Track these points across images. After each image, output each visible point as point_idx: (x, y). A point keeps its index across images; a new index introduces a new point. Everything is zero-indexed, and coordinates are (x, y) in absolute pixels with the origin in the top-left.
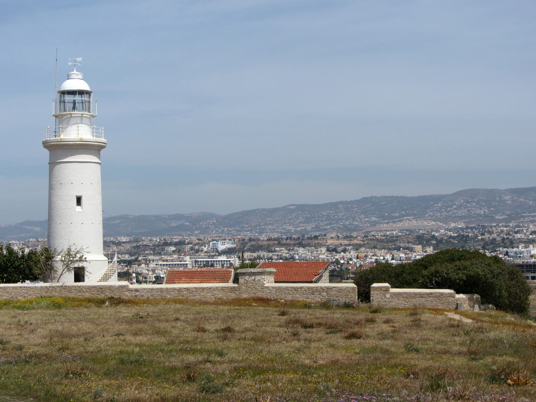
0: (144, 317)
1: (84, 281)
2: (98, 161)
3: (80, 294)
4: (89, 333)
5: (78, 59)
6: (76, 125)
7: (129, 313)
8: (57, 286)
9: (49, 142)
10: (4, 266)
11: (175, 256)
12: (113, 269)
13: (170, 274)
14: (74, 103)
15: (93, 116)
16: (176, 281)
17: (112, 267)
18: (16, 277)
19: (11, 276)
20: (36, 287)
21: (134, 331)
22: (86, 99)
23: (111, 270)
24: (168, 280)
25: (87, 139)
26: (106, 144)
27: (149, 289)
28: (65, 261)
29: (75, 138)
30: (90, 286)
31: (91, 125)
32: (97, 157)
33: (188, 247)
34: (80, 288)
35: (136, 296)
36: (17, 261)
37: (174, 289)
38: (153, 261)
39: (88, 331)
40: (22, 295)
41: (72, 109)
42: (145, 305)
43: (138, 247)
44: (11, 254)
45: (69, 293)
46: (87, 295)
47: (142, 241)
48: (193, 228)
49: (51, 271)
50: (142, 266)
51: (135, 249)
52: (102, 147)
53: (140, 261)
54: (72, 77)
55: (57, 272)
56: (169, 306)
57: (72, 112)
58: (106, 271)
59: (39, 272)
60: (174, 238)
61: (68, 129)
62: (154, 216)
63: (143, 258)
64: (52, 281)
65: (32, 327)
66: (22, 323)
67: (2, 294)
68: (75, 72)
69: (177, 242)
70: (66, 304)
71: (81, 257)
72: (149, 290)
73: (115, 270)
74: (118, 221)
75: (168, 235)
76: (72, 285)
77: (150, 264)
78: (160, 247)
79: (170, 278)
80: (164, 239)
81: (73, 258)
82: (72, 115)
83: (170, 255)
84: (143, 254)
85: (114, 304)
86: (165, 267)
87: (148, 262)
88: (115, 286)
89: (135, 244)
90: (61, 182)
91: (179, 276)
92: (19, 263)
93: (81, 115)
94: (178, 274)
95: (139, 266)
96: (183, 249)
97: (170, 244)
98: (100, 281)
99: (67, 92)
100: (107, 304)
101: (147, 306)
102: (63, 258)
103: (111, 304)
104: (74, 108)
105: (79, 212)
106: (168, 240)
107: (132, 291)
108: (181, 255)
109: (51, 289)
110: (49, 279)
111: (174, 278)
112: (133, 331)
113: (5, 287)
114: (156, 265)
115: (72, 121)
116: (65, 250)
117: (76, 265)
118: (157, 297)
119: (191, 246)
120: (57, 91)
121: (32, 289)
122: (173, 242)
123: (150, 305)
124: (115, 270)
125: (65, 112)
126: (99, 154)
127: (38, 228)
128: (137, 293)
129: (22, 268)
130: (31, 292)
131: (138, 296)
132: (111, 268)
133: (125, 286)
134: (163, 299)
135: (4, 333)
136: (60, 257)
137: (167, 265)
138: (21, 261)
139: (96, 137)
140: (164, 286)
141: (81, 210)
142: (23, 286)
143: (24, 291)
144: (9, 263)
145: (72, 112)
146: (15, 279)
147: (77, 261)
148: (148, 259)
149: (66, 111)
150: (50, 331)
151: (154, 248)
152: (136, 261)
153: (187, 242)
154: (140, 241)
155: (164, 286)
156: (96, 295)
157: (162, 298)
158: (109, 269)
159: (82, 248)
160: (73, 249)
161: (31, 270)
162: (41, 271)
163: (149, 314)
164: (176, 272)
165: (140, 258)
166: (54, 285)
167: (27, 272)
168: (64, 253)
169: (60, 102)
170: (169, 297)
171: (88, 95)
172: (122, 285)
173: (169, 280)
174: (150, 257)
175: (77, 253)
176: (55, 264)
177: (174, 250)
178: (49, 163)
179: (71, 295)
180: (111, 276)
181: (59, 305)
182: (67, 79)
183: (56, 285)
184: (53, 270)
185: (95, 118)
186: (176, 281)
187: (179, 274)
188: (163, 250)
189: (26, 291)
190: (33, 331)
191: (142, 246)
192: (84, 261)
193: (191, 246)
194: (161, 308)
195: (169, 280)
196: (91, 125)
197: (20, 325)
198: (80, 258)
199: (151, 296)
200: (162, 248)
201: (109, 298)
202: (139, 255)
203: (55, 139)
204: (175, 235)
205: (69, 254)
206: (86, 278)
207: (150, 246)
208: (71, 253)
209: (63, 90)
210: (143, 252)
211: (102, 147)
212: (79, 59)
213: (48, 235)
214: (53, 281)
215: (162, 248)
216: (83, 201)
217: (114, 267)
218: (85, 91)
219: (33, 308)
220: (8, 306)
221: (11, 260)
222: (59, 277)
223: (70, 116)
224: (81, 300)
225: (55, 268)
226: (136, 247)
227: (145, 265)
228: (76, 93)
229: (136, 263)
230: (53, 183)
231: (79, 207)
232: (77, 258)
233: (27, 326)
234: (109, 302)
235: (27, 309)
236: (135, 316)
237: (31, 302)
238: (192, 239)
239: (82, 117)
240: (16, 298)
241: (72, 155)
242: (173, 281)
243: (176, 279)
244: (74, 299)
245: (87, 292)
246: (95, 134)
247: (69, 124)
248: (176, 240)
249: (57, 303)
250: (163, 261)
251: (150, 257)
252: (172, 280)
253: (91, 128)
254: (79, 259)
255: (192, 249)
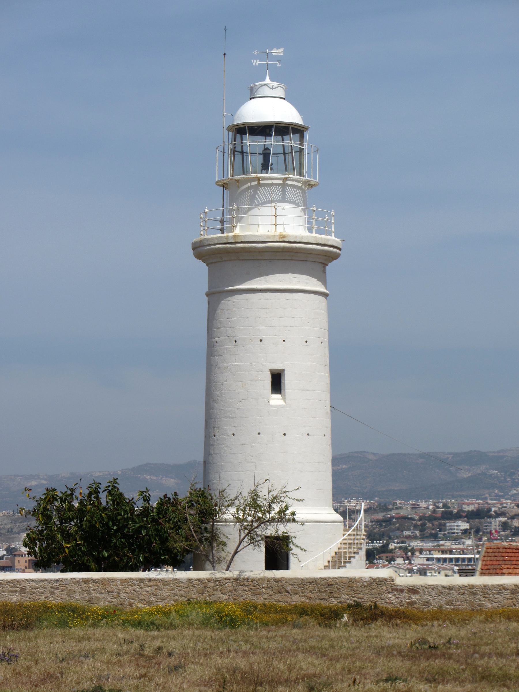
0: (440, 647)
1: (287, 568)
2: (321, 288)
3: (278, 597)
4: (314, 675)
5: (275, 50)
6: (270, 205)
7: (401, 639)
8: (226, 579)
9: (207, 243)
10: (103, 532)
11: (469, 542)
12: (356, 541)
13: (490, 554)
14: (266, 154)
15: (310, 185)
16: (504, 571)
17: (352, 537)
18: (129, 558)
19: (118, 555)
20: (176, 579)
21: (426, 673)
22: (294, 145)
23: (350, 544)
24: (486, 567)
25: (296, 237)
26: (340, 249)
27: (443, 587)
28: (244, 520)
29: (269, 233)
30: (302, 579)
31: (305, 205)
32: (319, 280)
33: (496, 523)
34: (280, 583)
35: (412, 603)
36: (133, 520)
37: (503, 588)
38: (421, 551)
39: (313, 672)
40: (143, 598)
41: (259, 167)
42: (435, 623)
43: (388, 521)
44: (118, 504)
45: (255, 594)
46: (296, 600)
47: (397, 509)
48: (507, 482)
49: (211, 544)
50: (396, 562)
51: (381, 525)
52: (331, 257)
53: (391, 551)
54: (261, 92)
55: (226, 546)
56: (492, 625)
57: (260, 175)
58: (339, 546)
59: (184, 544)
60: (464, 503)
61: (251, 213)
62: (422, 456)
63: (399, 545)
64: (213, 567)
65: (173, 661)
66: (148, 652)
67: (98, 595)
68: (268, 81)
69: (473, 511)
70: (248, 618)
71: (282, 512)
72: (443, 590)
73: (361, 544)
74: (344, 466)
75: (453, 497)
76: (262, 575)
77: (414, 558)
78: (436, 523)
79: (491, 563)
80: (445, 506)
81: (264, 513)
82: (261, 182)
83: (456, 539)
84: (398, 537)
85: (362, 619)
86: (446, 565)
87: (409, 554)
88: (361, 579)
89: (380, 516)
90: (235, 338)
91: (512, 559)
92: (138, 525)
93: (281, 182)
94: (510, 554)
95: (389, 562)
96: (486, 526)
97: (458, 516)
98: (326, 567)
99: (248, 127)
100: (346, 618)
101: (440, 625)
102: (241, 514)
103: (355, 621)
104: (265, 167)
105: (278, 407)
106: (454, 507)
107: (402, 591)
108: (480, 540)
109: (211, 584)
110: (208, 563)
111: (500, 563)
112: (424, 673)
113: (104, 579)
114: (428, 559)
115: (262, 194)
116: (246, 493)
117: (270, 531)
118: (461, 607)
119: (503, 519)
120: (226, 126)
121: (167, 585)
122: (464, 511)
123: (448, 622)
124: (361, 544)
125: (244, 174)
126: (324, 272)
127: (172, 480)
128: (415, 598)
129: (144, 536)
130: (165, 593)
131: (415, 603)
132: (350, 539)
133: (385, 580)
134: (477, 611)
135: (105, 673)
136: (233, 510)
137: (451, 560)
138: (143, 521)
139: (316, 233)
140: (477, 580)
141: (281, 402)
142: (147, 577)
143: (148, 589)
144: (113, 525)
145: (260, 175)
146: (128, 563)
147: (273, 520)
148: (409, 548)
149: (248, 173)
150: (219, 670)
151: (424, 525)
152: (383, 552)
153: (495, 512)
154: (391, 510)
155: (477, 580)
156: (318, 601)
157: (473, 610)
158: (345, 541)
159: (284, 490)
160: (264, 492)
161: (164, 541)
162: (189, 543)
163: (452, 640)
164: (504, 550)
165: (392, 546)
166: (219, 575)
167: (156, 545)
168: (242, 501)
169: (234, 151)
170: (489, 606)
171: (298, 135)
172: (378, 578)
173: (489, 567)
174: (415, 544)
175: (273, 502)
176: (222, 528)
177: (465, 528)
178: (207, 295)
179: (259, 600)
180: (350, 558)
181: (232, 620)
182: (249, 98)
183: (223, 576)
184: (216, 540)
185: (314, 188)
186: (504, 571)
187: (513, 555)
188: (442, 527)
189: (154, 589)
190: (176, 668)
191: (396, 518)
192: (289, 521)
193: (503, 519)
194: (474, 630)
195: (489, 567)
196: (305, 204)
197: (142, 655)
198: (280, 513)
199: (448, 603)
200: (440, 525)
201: (350, 606)
202: (390, 538)
203: (222, 237)
204: (467, 497)
205: (254, 504)
206: (292, 560)
207: (414, 520)
208: (259, 502)
209: (239, 122)
210: (398, 533)
211: (331, 257)
212: (278, 52)
213: (205, 462)
214: (217, 566)
215: (440, 525)
216: (288, 381)
217: (359, 537)
218: (292, 124)
219: (172, 626)
220: (112, 621)
221: (119, 517)
222: (229, 558)
223: (256, 183)
224: (282, 611)
225: (221, 536)
226: (383, 521)
227: (404, 560)
228: (271, 131)
229: (384, 555)
230: (217, 339)
231: (278, 396)
232: (273, 514)
233: (160, 658)
234: (350, 614)
235: (158, 627)
236: (417, 645)
237: (166, 614)
238: (505, 505)
239: (284, 186)
240: (131, 605)
241: (260, 275)
242: (498, 571)
243: (506, 566)
244: (266, 609)
245: (296, 593)
246: (314, 226)
247: (253, 202)
248: (471, 508)
249: (226, 616)
250: (443, 552)
251: (415, 544)
252: (496, 567)
253: (304, 210)
254: (277, 516)
255: (505, 526)
